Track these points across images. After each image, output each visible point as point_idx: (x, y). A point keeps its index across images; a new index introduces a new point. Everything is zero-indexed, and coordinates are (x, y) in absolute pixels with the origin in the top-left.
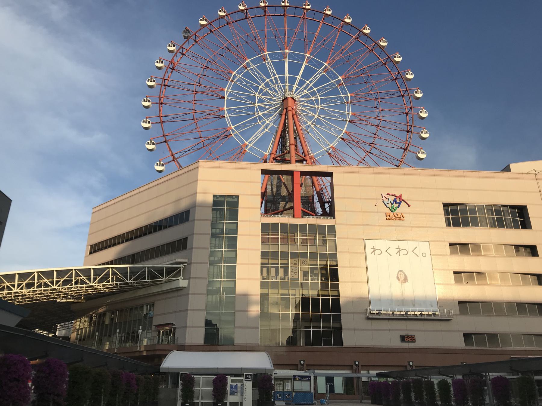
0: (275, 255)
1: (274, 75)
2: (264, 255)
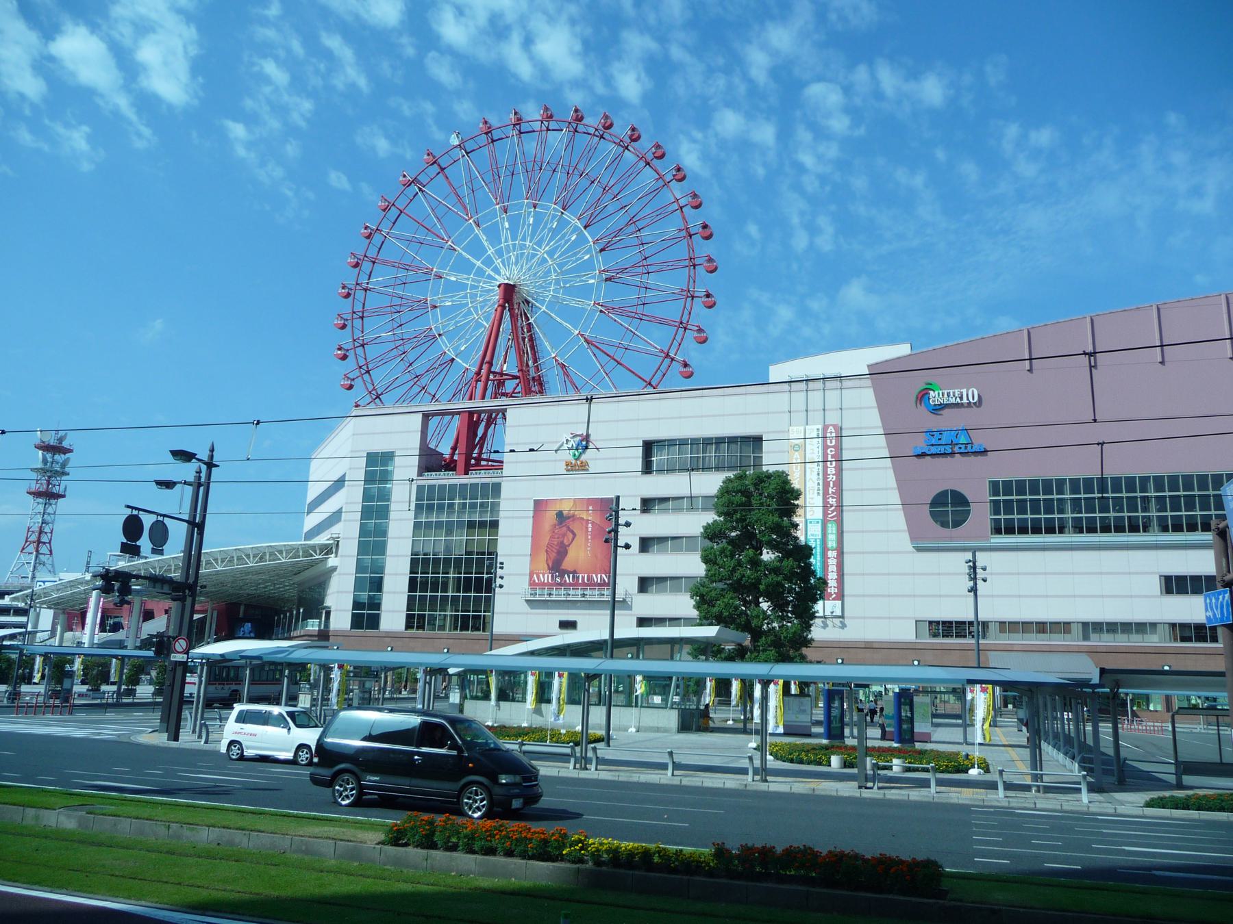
0: (428, 525)
1: (468, 279)
2: (417, 526)
